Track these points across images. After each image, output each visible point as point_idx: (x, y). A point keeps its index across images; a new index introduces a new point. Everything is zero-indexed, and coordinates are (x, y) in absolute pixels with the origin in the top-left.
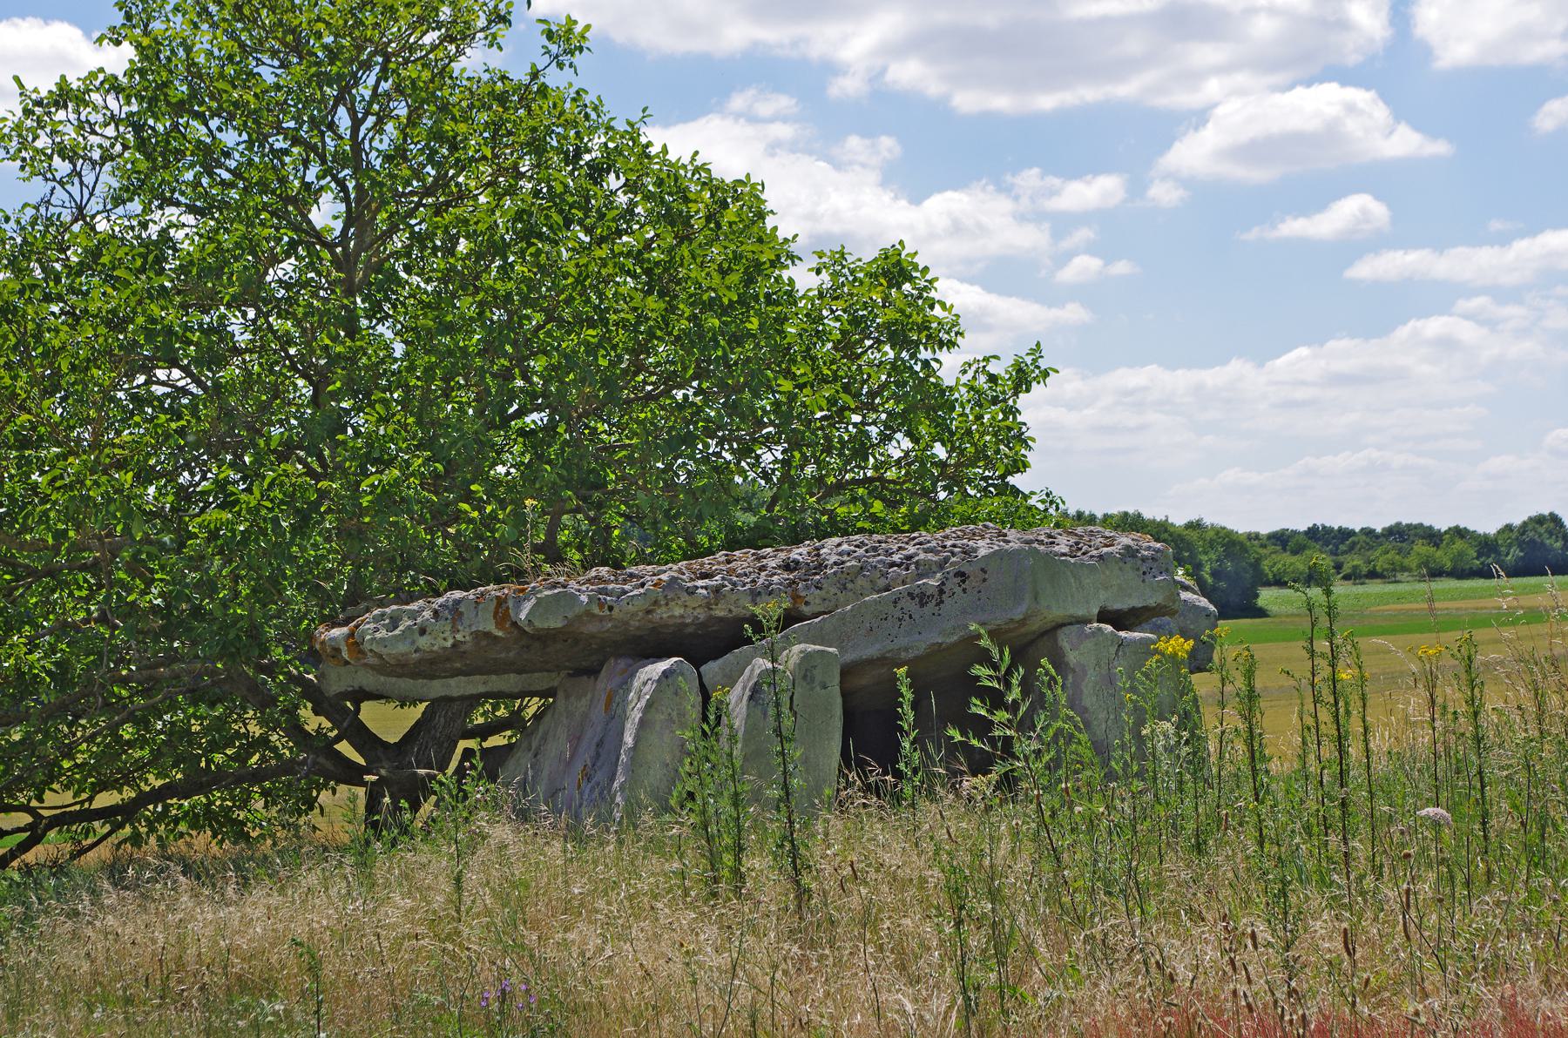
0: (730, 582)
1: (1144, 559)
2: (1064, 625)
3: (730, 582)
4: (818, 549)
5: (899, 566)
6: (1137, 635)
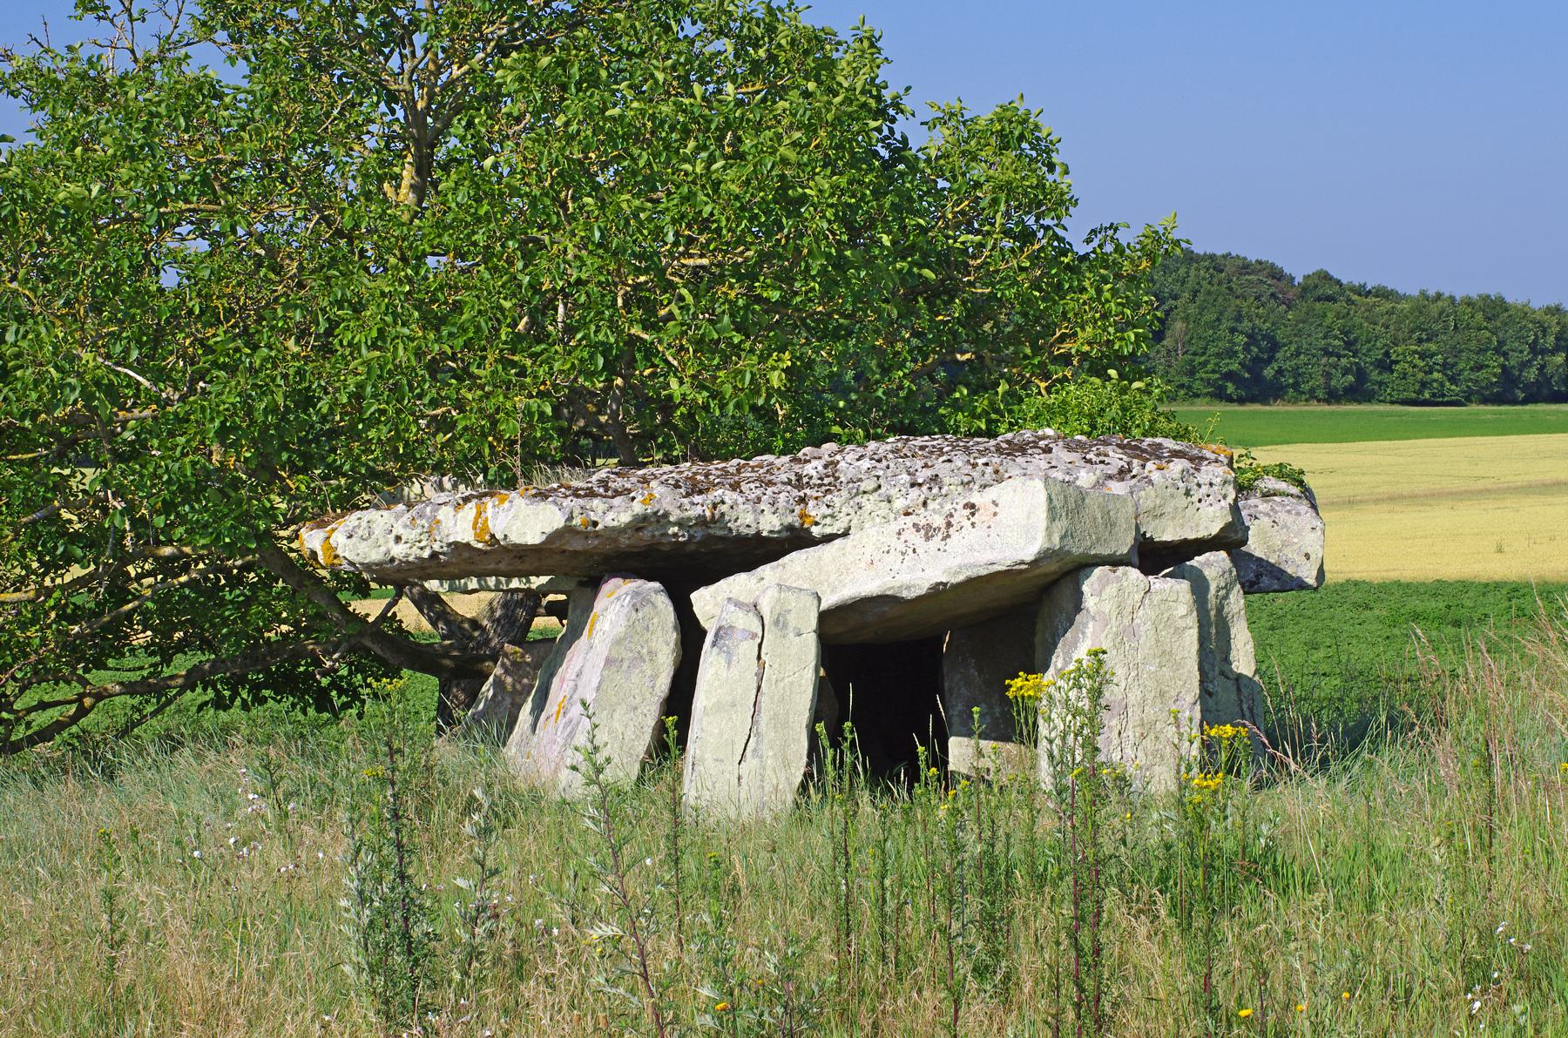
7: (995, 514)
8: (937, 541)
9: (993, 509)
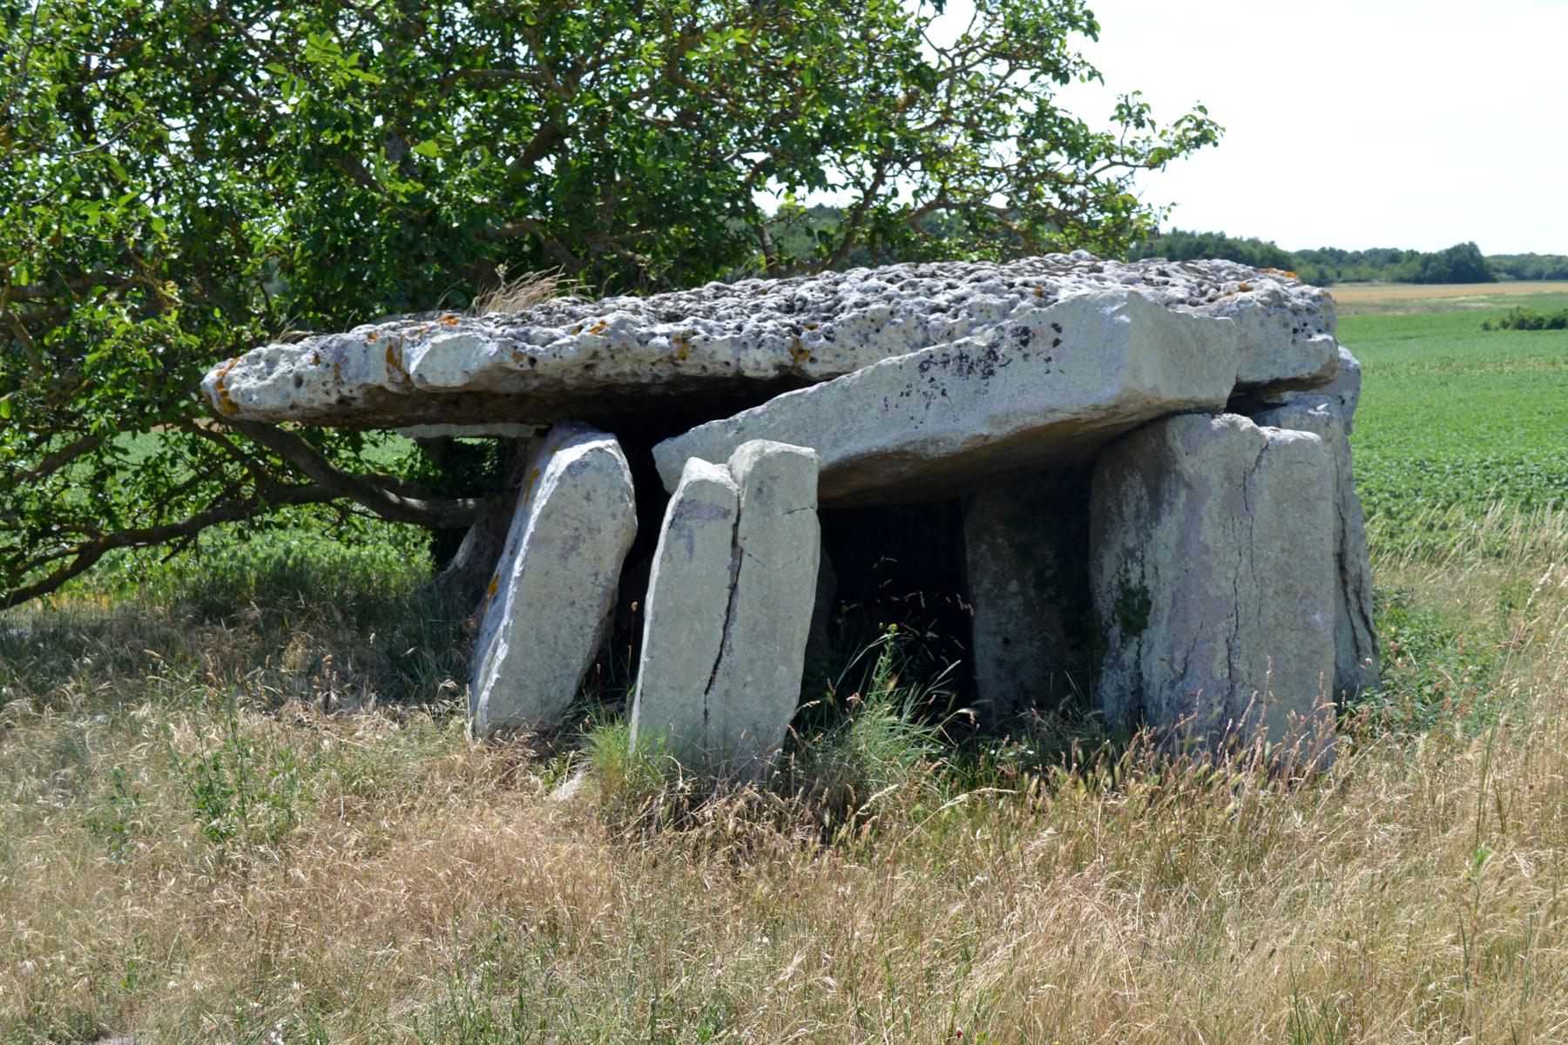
0: (705, 327)
1: (1296, 311)
2: (1177, 413)
3: (705, 327)
4: (837, 283)
5: (943, 311)
6: (1288, 434)
7: (1056, 343)
8: (976, 376)
9: (1054, 335)
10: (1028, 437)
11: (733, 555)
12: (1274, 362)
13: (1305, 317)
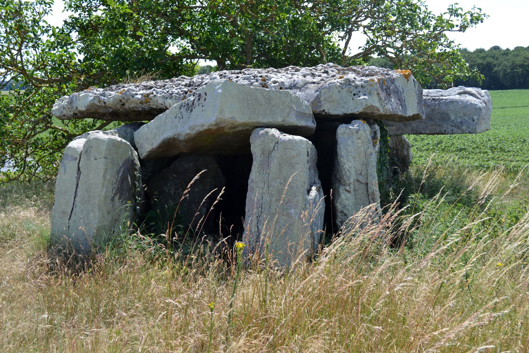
1: (356, 87)
10: (200, 134)
11: (77, 173)
12: (344, 107)
13: (360, 89)
